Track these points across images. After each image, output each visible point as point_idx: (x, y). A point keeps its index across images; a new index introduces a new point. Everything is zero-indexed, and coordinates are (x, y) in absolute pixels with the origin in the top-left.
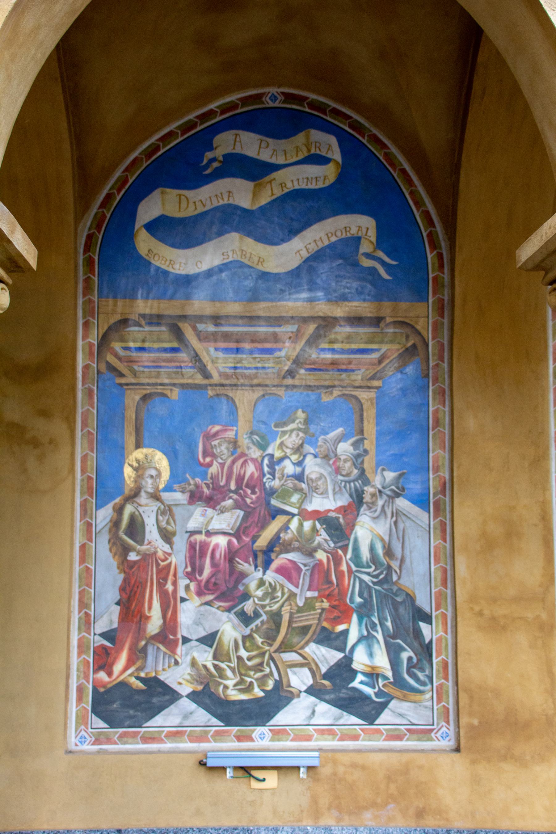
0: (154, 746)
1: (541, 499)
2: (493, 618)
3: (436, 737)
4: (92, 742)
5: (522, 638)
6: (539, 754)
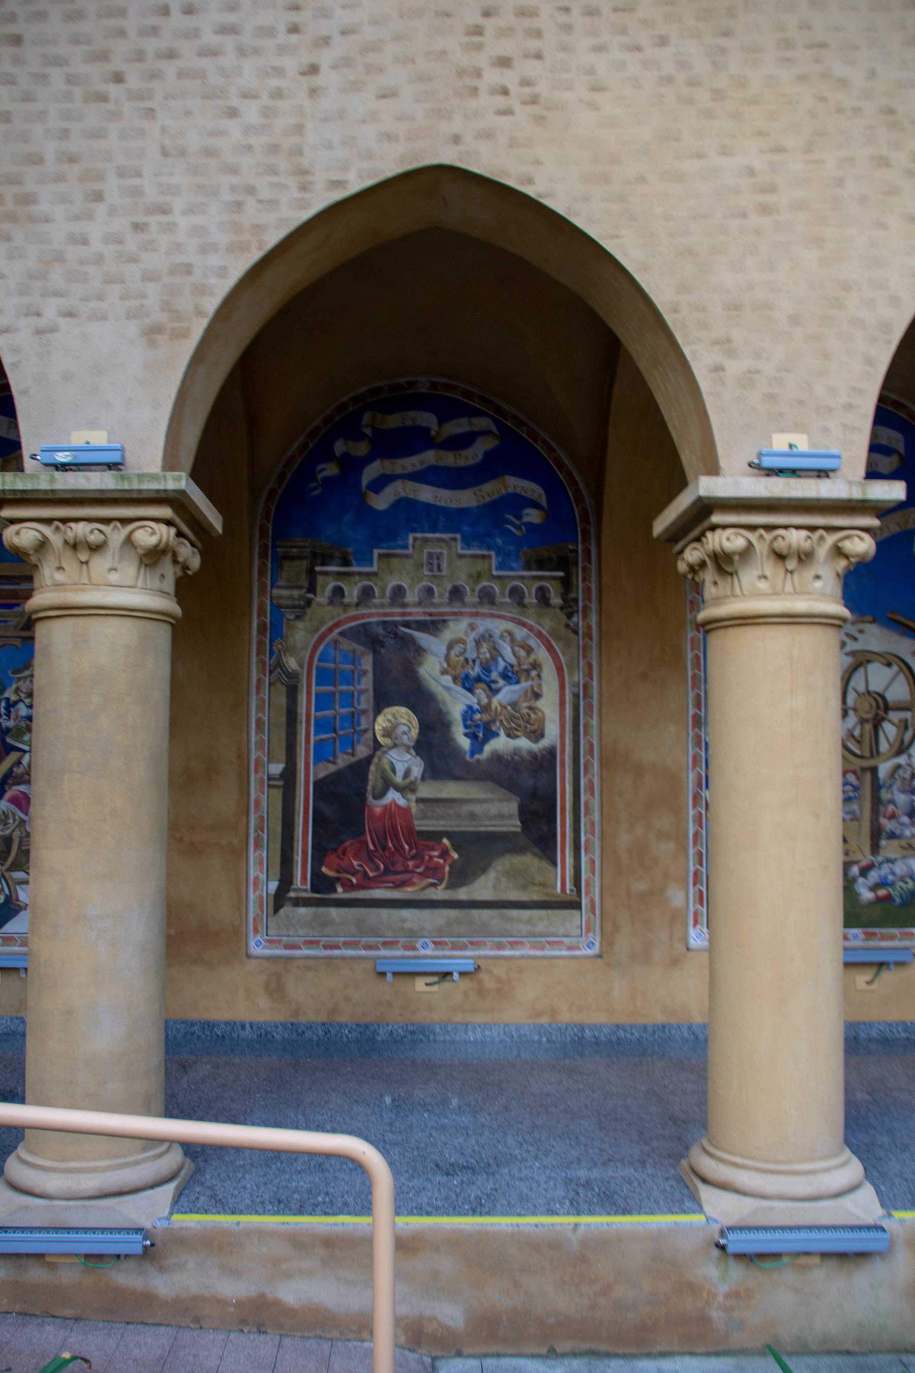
0: (336, 952)
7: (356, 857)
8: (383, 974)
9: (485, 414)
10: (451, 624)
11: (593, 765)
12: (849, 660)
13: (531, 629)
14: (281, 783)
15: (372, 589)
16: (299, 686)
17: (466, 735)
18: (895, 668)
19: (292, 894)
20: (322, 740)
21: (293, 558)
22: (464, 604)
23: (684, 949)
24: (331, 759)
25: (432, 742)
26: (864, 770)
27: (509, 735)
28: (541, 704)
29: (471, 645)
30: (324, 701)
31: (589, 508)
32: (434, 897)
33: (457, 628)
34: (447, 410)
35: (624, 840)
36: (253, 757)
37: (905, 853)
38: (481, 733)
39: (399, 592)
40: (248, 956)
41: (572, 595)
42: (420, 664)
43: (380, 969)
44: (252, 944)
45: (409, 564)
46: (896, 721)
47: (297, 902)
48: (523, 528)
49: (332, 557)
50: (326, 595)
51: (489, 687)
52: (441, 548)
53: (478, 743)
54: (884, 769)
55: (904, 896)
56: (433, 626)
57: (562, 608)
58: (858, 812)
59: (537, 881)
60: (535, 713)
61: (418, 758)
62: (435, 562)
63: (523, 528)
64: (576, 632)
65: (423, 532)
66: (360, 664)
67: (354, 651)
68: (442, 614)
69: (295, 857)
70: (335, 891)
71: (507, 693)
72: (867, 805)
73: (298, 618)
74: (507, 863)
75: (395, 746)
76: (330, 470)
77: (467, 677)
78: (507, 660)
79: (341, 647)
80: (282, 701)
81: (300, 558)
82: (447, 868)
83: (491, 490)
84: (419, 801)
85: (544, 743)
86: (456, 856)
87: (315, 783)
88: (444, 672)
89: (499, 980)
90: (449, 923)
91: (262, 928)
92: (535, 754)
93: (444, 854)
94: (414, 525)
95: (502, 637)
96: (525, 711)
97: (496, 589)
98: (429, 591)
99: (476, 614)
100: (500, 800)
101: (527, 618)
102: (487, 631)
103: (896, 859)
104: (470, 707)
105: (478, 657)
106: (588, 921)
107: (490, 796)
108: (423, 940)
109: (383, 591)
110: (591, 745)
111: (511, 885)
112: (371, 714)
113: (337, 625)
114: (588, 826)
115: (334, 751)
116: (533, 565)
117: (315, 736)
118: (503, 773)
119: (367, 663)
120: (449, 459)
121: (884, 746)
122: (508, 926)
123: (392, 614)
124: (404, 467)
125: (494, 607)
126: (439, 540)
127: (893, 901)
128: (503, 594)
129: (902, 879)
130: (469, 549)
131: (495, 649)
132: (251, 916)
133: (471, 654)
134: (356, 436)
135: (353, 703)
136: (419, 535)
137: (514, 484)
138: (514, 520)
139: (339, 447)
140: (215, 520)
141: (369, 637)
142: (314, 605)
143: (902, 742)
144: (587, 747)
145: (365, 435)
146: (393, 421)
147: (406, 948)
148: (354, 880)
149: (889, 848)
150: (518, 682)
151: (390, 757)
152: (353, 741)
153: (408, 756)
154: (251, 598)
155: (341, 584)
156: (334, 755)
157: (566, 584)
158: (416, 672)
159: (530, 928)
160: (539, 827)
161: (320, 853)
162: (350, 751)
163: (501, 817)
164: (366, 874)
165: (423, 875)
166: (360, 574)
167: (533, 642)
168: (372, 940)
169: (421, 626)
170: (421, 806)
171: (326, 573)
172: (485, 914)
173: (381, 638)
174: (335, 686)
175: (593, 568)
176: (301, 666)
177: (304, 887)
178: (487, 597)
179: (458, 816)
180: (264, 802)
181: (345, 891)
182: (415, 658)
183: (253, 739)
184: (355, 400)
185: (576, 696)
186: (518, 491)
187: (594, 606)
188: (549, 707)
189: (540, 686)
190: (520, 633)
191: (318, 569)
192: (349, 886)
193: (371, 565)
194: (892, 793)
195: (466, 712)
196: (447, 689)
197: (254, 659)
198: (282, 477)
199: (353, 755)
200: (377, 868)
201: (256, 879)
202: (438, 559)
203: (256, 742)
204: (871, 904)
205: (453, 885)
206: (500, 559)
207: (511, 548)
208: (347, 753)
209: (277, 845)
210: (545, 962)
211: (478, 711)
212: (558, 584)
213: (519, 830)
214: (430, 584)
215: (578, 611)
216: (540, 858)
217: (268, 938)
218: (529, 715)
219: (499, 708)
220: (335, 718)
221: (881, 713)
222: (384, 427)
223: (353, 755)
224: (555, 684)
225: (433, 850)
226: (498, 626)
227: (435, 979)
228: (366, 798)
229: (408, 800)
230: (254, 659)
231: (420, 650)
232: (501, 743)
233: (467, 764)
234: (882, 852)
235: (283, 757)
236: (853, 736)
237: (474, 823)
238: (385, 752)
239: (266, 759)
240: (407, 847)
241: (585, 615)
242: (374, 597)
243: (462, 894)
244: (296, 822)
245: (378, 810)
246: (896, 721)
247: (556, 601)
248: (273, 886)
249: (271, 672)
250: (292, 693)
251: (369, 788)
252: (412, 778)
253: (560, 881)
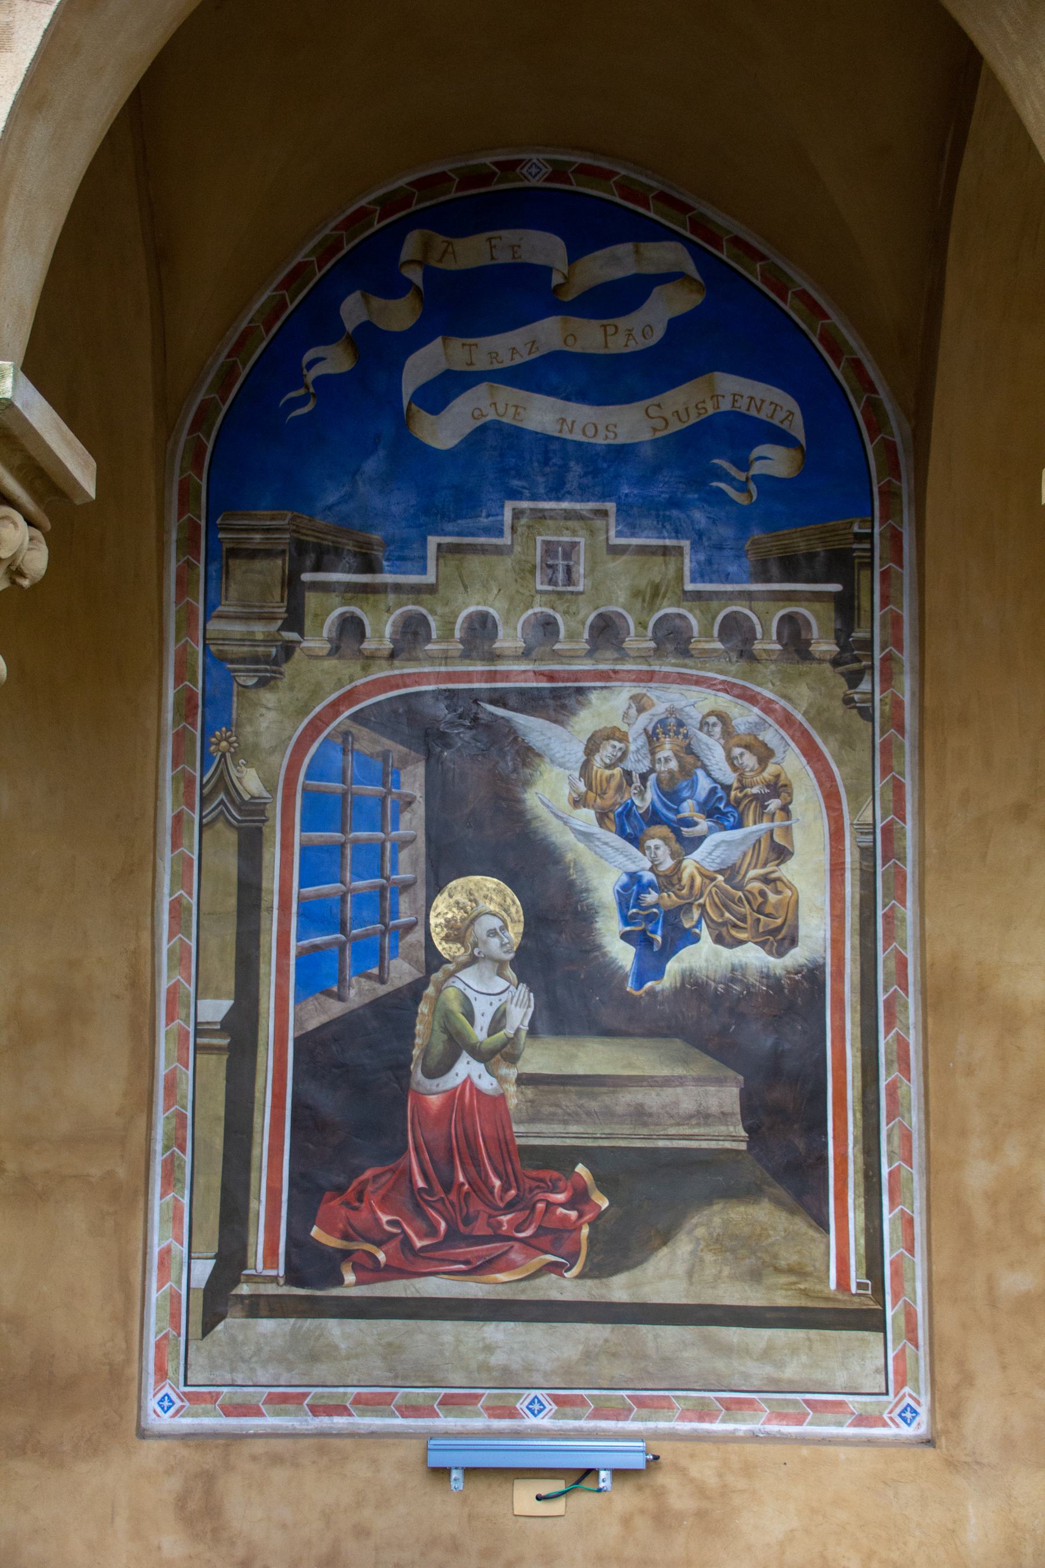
0: (339, 1422)
1: (132, 947)
2: (24, 1178)
3: (891, 1419)
4: (550, 1414)
5: (76, 1216)
6: (89, 1440)
7: (385, 1203)
8: (442, 1473)
9: (671, 235)
10: (593, 696)
11: (906, 1006)
13: (768, 708)
14: (224, 1042)
15: (423, 621)
16: (266, 830)
17: (625, 937)
19: (244, 1289)
20: (316, 947)
21: (253, 554)
22: (623, 656)
24: (335, 989)
25: (554, 928)
27: (719, 940)
28: (788, 871)
29: (636, 743)
30: (317, 864)
31: (898, 440)
32: (555, 1295)
33: (607, 707)
34: (588, 225)
35: (978, 1176)
36: (164, 984)
38: (659, 932)
39: (482, 628)
40: (142, 1433)
41: (859, 634)
42: (527, 783)
43: (436, 1459)
44: (152, 1403)
45: (504, 566)
47: (255, 1307)
48: (752, 487)
49: (338, 551)
50: (325, 634)
51: (677, 832)
52: (574, 533)
53: (652, 963)
56: (557, 701)
57: (836, 662)
59: (783, 1263)
60: (778, 892)
61: (523, 988)
62: (561, 563)
63: (752, 487)
64: (867, 714)
65: (534, 498)
66: (397, 784)
67: (385, 755)
68: (576, 676)
69: (253, 1204)
70: (340, 1281)
71: (716, 848)
73: (263, 683)
74: (717, 1220)
75: (473, 960)
76: (333, 360)
77: (628, 811)
78: (716, 774)
79: (357, 746)
80: (229, 863)
81: (269, 554)
82: (585, 1231)
83: (684, 404)
84: (523, 1080)
85: (797, 956)
86: (604, 1203)
87: (297, 1040)
88: (578, 802)
89: (701, 1491)
90: (588, 1356)
91: (174, 1367)
92: (778, 980)
93: (579, 1199)
94: (516, 483)
95: (703, 725)
96: (756, 885)
97: (694, 622)
98: (548, 626)
99: (650, 677)
100: (699, 1081)
101: (760, 685)
102: (672, 711)
104: (634, 877)
105: (652, 770)
106: (900, 1357)
107: (680, 1071)
108: (534, 1393)
109: (448, 626)
110: (902, 963)
111: (726, 1271)
112: (421, 892)
113: (349, 698)
114: (896, 1140)
115: (342, 971)
116: (775, 570)
117: (298, 940)
118: (708, 1021)
119: (413, 781)
120: (591, 337)
122: (720, 1364)
123: (468, 677)
124: (493, 355)
125: (688, 661)
126: (568, 515)
128: (706, 634)
130: (633, 535)
131: (689, 750)
132: (152, 1339)
133: (637, 764)
134: (393, 287)
135: (382, 869)
136: (525, 505)
137: (733, 391)
138: (733, 471)
139: (353, 310)
140: (81, 469)
141: (416, 726)
142: (297, 654)
144: (892, 965)
145: (410, 284)
146: (471, 252)
147: (496, 1412)
148: (381, 1257)
150: (739, 825)
151: (462, 986)
152: (382, 949)
153: (501, 984)
154: (162, 640)
155: (358, 611)
156: (342, 981)
157: (846, 608)
158: (521, 801)
159: (769, 1370)
160: (787, 1142)
161: (307, 1195)
162: (375, 971)
163: (703, 1116)
164: (407, 1242)
165: (531, 1245)
166: (398, 588)
167: (772, 736)
168: (419, 1394)
169: (530, 702)
170: (530, 1092)
171: (325, 587)
172: (670, 1334)
173: (442, 727)
174: (343, 831)
175: (907, 574)
176: (270, 785)
177: (273, 1273)
178: (673, 639)
179: (609, 1115)
180: (186, 1081)
181: (359, 1283)
182: (515, 770)
183: (165, 947)
184: (388, 204)
185: (867, 853)
186: (742, 406)
187: (907, 657)
188: (806, 875)
189: (788, 830)
190: (744, 717)
191: (306, 577)
192: (371, 1271)
193: (424, 570)
195: (625, 887)
196: (586, 837)
197: (168, 773)
198: (228, 375)
199: (382, 980)
200: (432, 1230)
201: (166, 1254)
202: (567, 556)
203: (171, 952)
205: (600, 1268)
206: (702, 557)
207: (726, 532)
208: (369, 977)
209: (213, 1179)
210: (805, 1451)
211: (651, 885)
212: (828, 610)
213: (743, 1146)
214: (551, 612)
215: (872, 667)
216: (792, 1212)
217: (187, 1389)
218: (763, 894)
219: (698, 880)
220: (343, 899)
222: (450, 265)
223: (382, 980)
224: (822, 828)
225: (554, 1190)
226: (696, 702)
227: (559, 1485)
228: (409, 1074)
229: (502, 1080)
230: (168, 773)
231: (528, 755)
232: (702, 957)
233: (631, 1002)
235: (230, 985)
237: (645, 1131)
238: (452, 974)
239: (192, 989)
240: (497, 1183)
241: (888, 679)
242: (428, 639)
243: (619, 1289)
244: (257, 1126)
245: (435, 1101)
247: (824, 646)
248: (203, 1270)
249: (204, 801)
250: (251, 846)
251: (416, 1052)
252: (509, 1031)
253: (834, 1261)
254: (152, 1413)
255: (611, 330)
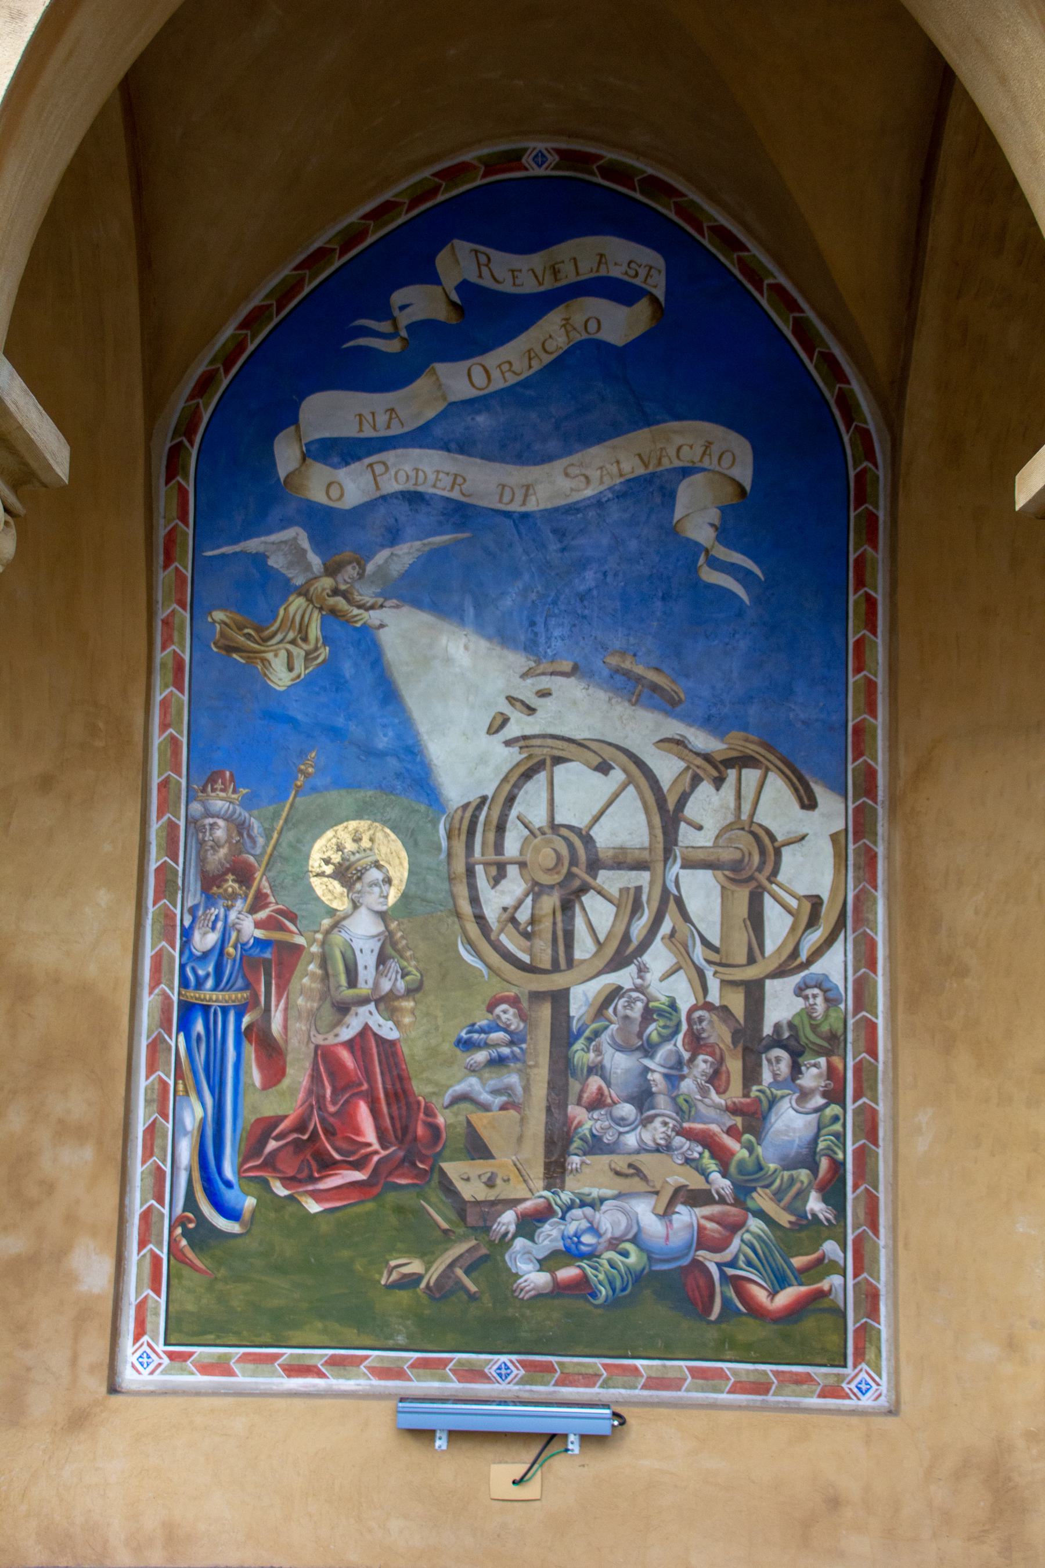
12: (513, 756)
18: (618, 776)
23: (104, 1389)
26: (536, 997)
37: (623, 1184)
46: (614, 892)
54: (582, 997)
55: (618, 1284)
58: (519, 1090)
72: (541, 1074)
103: (602, 1200)
121: (584, 948)
127: (594, 1295)
129: (614, 1244)
143: (626, 938)
149: (588, 1175)
194: (598, 1051)
204: (540, 1296)
221: (580, 871)
234: (570, 1180)
236: (513, 920)
246: (614, 892)
254: (129, 1367)
255: (379, 469)
